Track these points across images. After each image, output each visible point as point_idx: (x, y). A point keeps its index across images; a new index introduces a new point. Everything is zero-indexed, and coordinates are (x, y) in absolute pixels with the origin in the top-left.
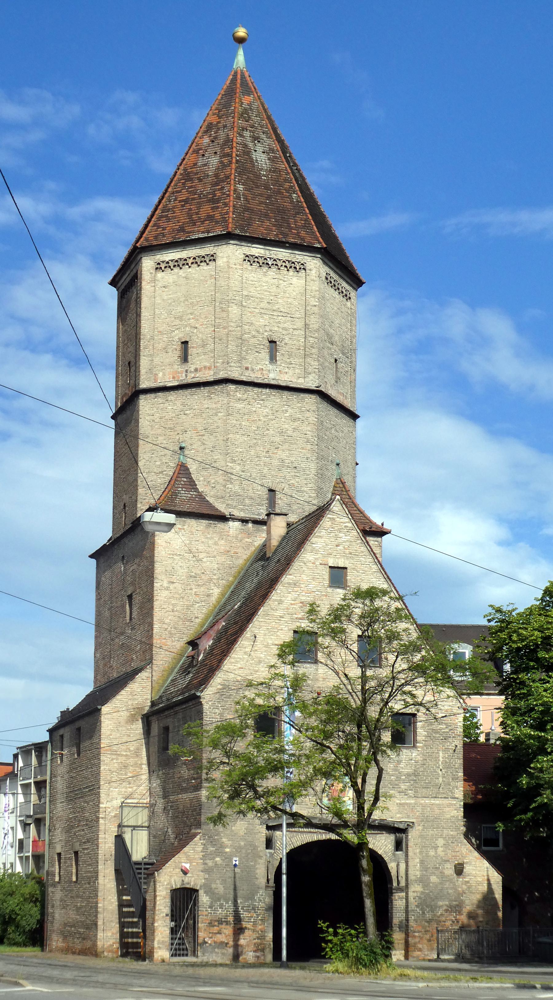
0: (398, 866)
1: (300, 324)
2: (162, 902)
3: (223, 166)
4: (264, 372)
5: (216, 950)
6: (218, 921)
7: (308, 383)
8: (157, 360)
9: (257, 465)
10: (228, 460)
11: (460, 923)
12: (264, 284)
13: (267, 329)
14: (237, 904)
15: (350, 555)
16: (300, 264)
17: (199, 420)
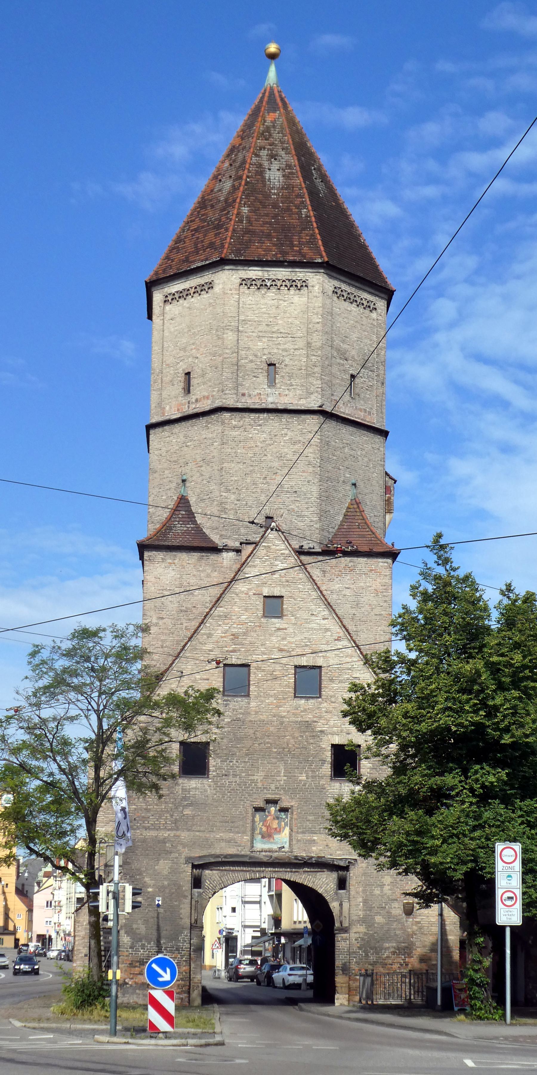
0: (341, 905)
1: (301, 343)
2: (81, 942)
3: (234, 189)
4: (262, 397)
5: (137, 991)
6: (139, 962)
7: (310, 403)
8: (165, 394)
9: (253, 493)
10: (222, 489)
11: (410, 966)
12: (263, 307)
13: (266, 352)
14: (161, 944)
15: (287, 583)
16: (301, 281)
17: (198, 451)
